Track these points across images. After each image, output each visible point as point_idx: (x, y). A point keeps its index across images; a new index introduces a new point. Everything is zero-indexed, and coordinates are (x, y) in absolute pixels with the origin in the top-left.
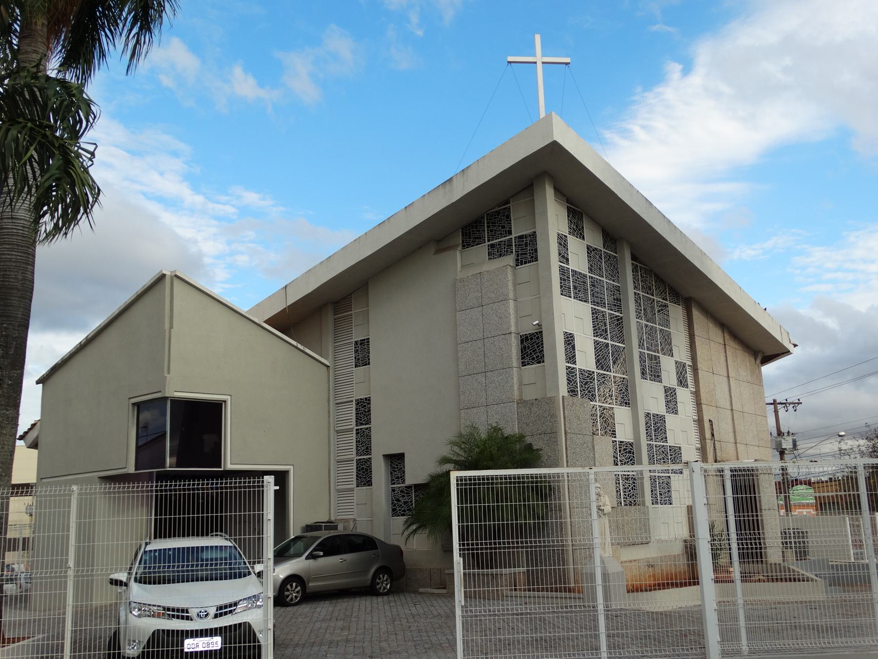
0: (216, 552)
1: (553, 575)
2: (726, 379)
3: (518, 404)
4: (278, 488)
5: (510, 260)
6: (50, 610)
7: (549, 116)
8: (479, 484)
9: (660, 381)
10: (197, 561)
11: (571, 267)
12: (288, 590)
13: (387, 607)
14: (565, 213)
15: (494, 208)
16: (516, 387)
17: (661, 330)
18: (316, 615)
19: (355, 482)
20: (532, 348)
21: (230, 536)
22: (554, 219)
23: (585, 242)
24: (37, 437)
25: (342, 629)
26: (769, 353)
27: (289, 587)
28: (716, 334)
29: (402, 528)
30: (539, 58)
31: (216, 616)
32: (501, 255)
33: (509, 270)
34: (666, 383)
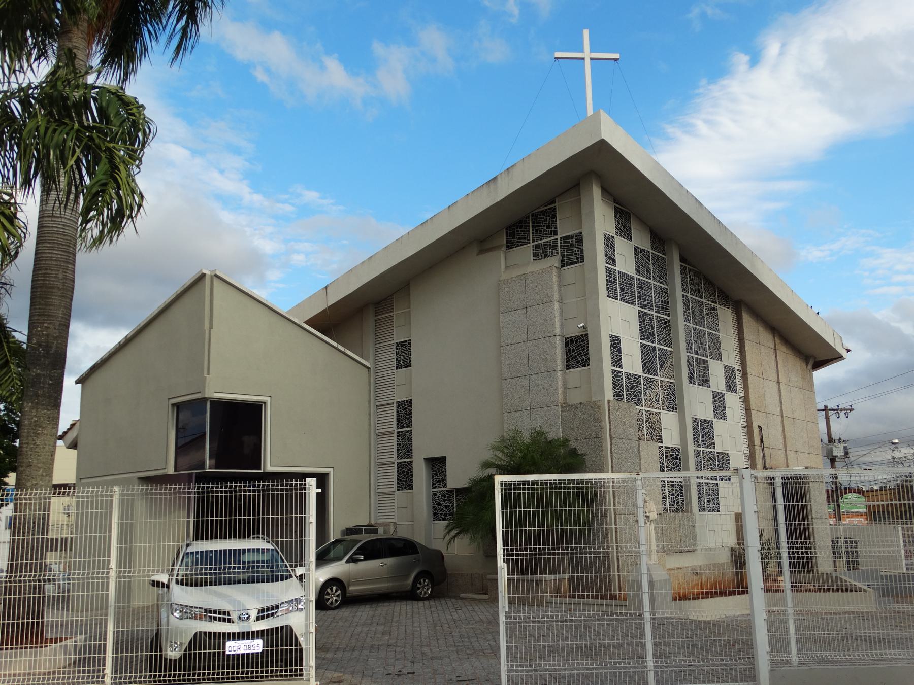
1: (596, 582)
2: (776, 384)
3: (562, 407)
4: (320, 490)
5: (555, 261)
7: (596, 114)
9: (709, 386)
10: (239, 563)
11: (617, 269)
12: (328, 594)
15: (539, 208)
16: (560, 391)
17: (710, 334)
18: (356, 619)
19: (395, 486)
20: (577, 351)
22: (601, 219)
23: (633, 243)
24: (77, 437)
26: (821, 358)
27: (329, 590)
28: (766, 338)
29: (443, 533)
30: (587, 54)
31: (258, 619)
33: (555, 272)
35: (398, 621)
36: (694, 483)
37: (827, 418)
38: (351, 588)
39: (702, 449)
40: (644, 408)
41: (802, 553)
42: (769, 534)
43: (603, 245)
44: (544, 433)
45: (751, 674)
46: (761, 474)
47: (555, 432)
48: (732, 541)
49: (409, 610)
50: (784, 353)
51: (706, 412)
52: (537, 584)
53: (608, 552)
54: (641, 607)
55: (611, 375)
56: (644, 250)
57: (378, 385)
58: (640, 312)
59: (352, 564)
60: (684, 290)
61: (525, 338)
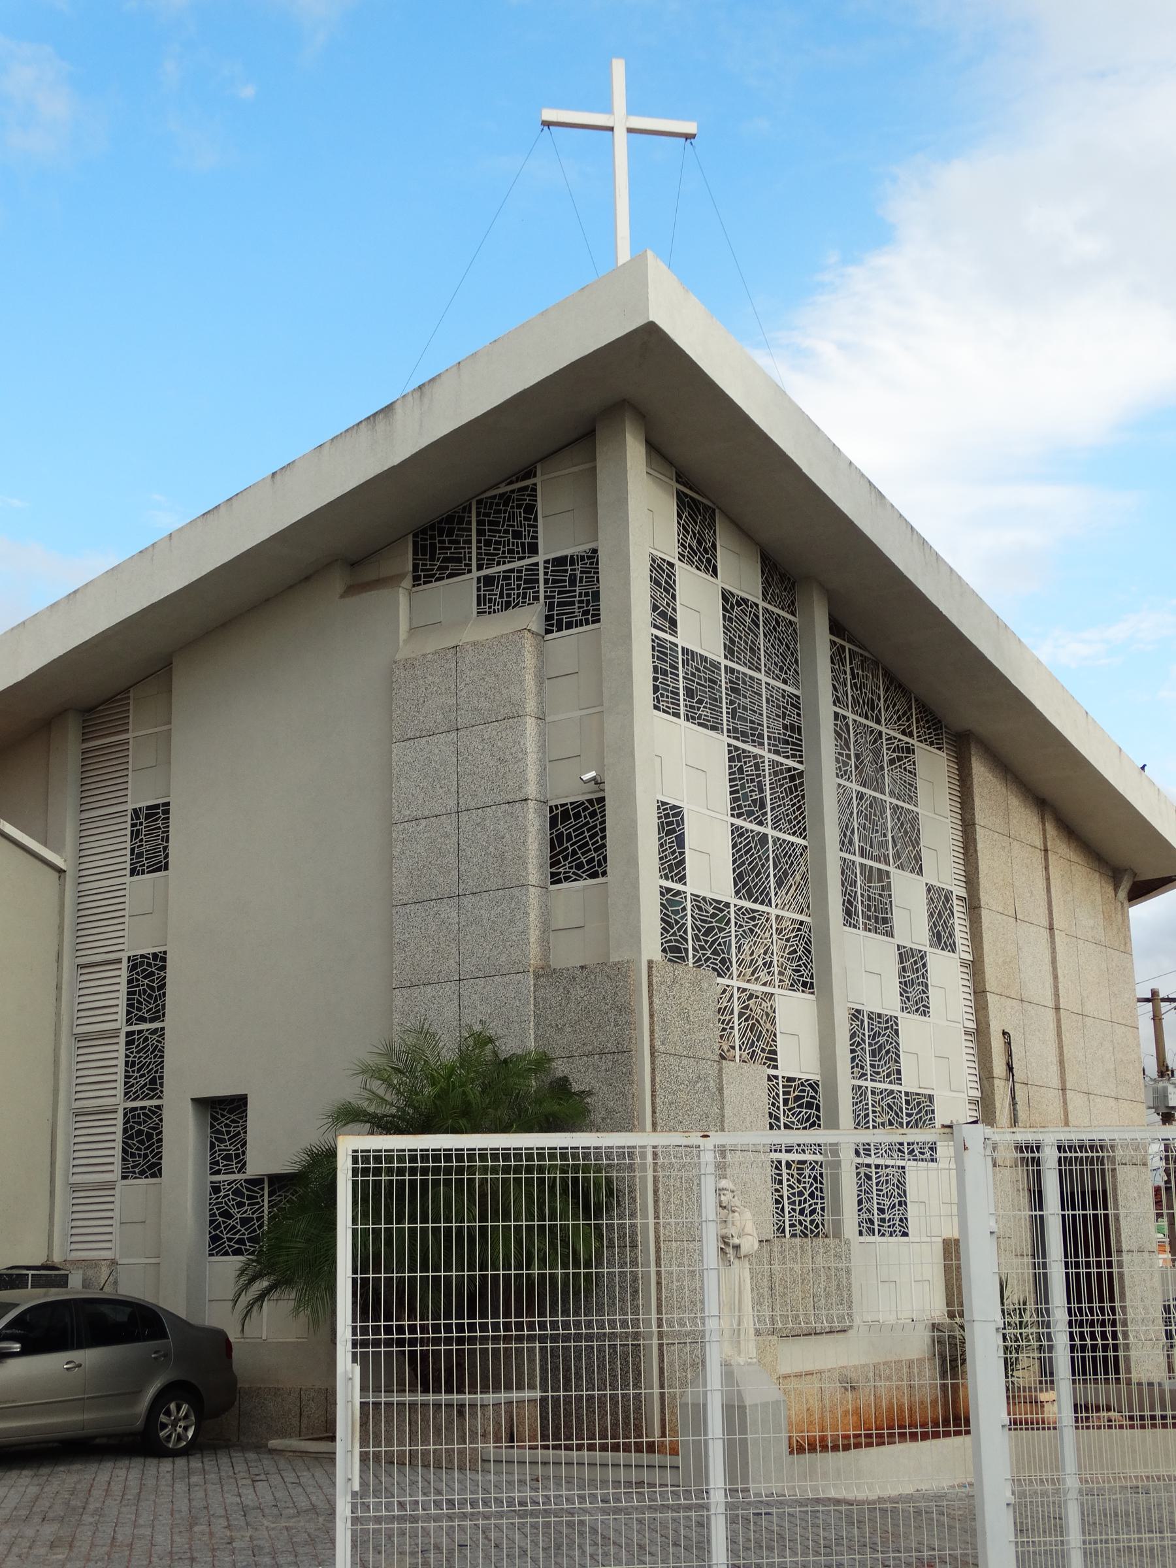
1: (608, 1409)
2: (1045, 934)
3: (537, 977)
5: (531, 616)
7: (639, 260)
9: (890, 933)
16: (534, 935)
17: (895, 808)
19: (117, 1168)
20: (579, 838)
22: (643, 519)
23: (720, 583)
25: (52, 1546)
26: (1148, 874)
28: (1025, 823)
30: (620, 118)
32: (508, 605)
33: (529, 643)
35: (99, 1512)
36: (848, 1160)
37: (1157, 1019)
39: (870, 1084)
41: (1093, 1336)
42: (1022, 1289)
43: (648, 584)
44: (490, 1040)
46: (1006, 1136)
47: (519, 1039)
48: (937, 1309)
49: (133, 1483)
51: (883, 997)
52: (461, 1413)
53: (636, 1336)
54: (702, 1473)
56: (745, 601)
57: (83, 915)
58: (732, 749)
60: (837, 701)
61: (451, 804)
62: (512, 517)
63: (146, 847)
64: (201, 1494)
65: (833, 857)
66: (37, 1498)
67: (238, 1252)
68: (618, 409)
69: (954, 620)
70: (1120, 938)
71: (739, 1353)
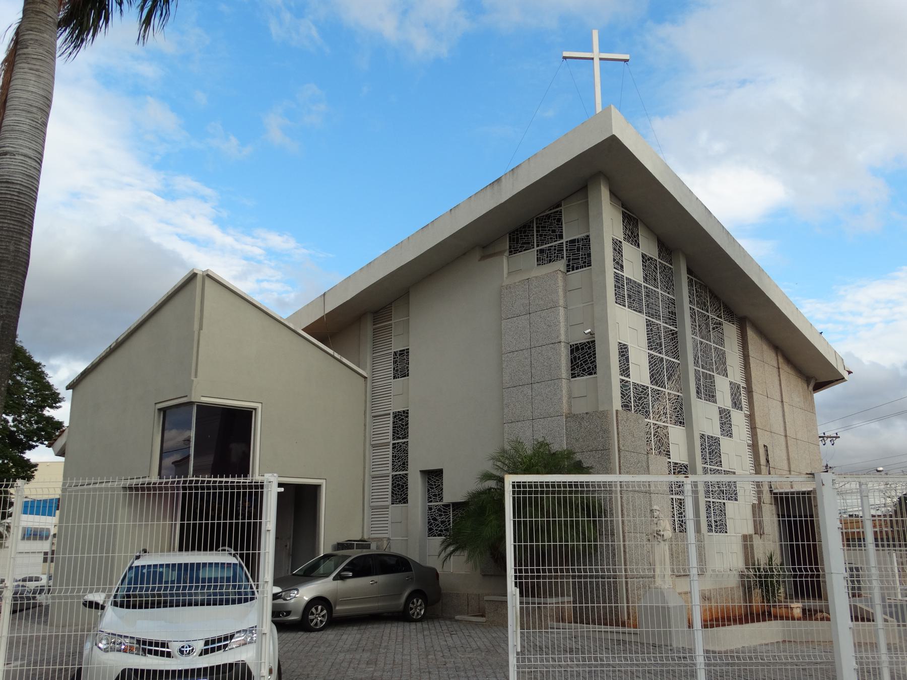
0: (210, 571)
1: (602, 608)
2: (780, 404)
3: (567, 418)
5: (561, 265)
6: (70, 625)
7: (607, 110)
8: (542, 492)
9: (715, 402)
10: (197, 582)
11: (625, 275)
12: (312, 614)
13: (420, 636)
14: (620, 218)
15: (544, 212)
17: (716, 348)
18: (341, 644)
19: (390, 499)
20: (584, 358)
21: (236, 550)
22: (609, 223)
23: (642, 250)
24: (65, 445)
25: (368, 663)
26: (823, 379)
27: (313, 610)
28: (770, 356)
29: (438, 549)
30: (596, 54)
31: (206, 652)
32: (550, 261)
33: (560, 275)
34: (720, 404)
38: (337, 608)
40: (651, 421)
45: (693, 674)
49: (400, 634)
50: (787, 373)
51: (713, 429)
55: (619, 385)
59: (339, 582)
62: (551, 224)
63: (399, 367)
64: (429, 640)
65: (692, 368)
66: (360, 640)
67: (440, 535)
68: (597, 176)
69: (742, 267)
70: (810, 406)
71: (665, 583)
